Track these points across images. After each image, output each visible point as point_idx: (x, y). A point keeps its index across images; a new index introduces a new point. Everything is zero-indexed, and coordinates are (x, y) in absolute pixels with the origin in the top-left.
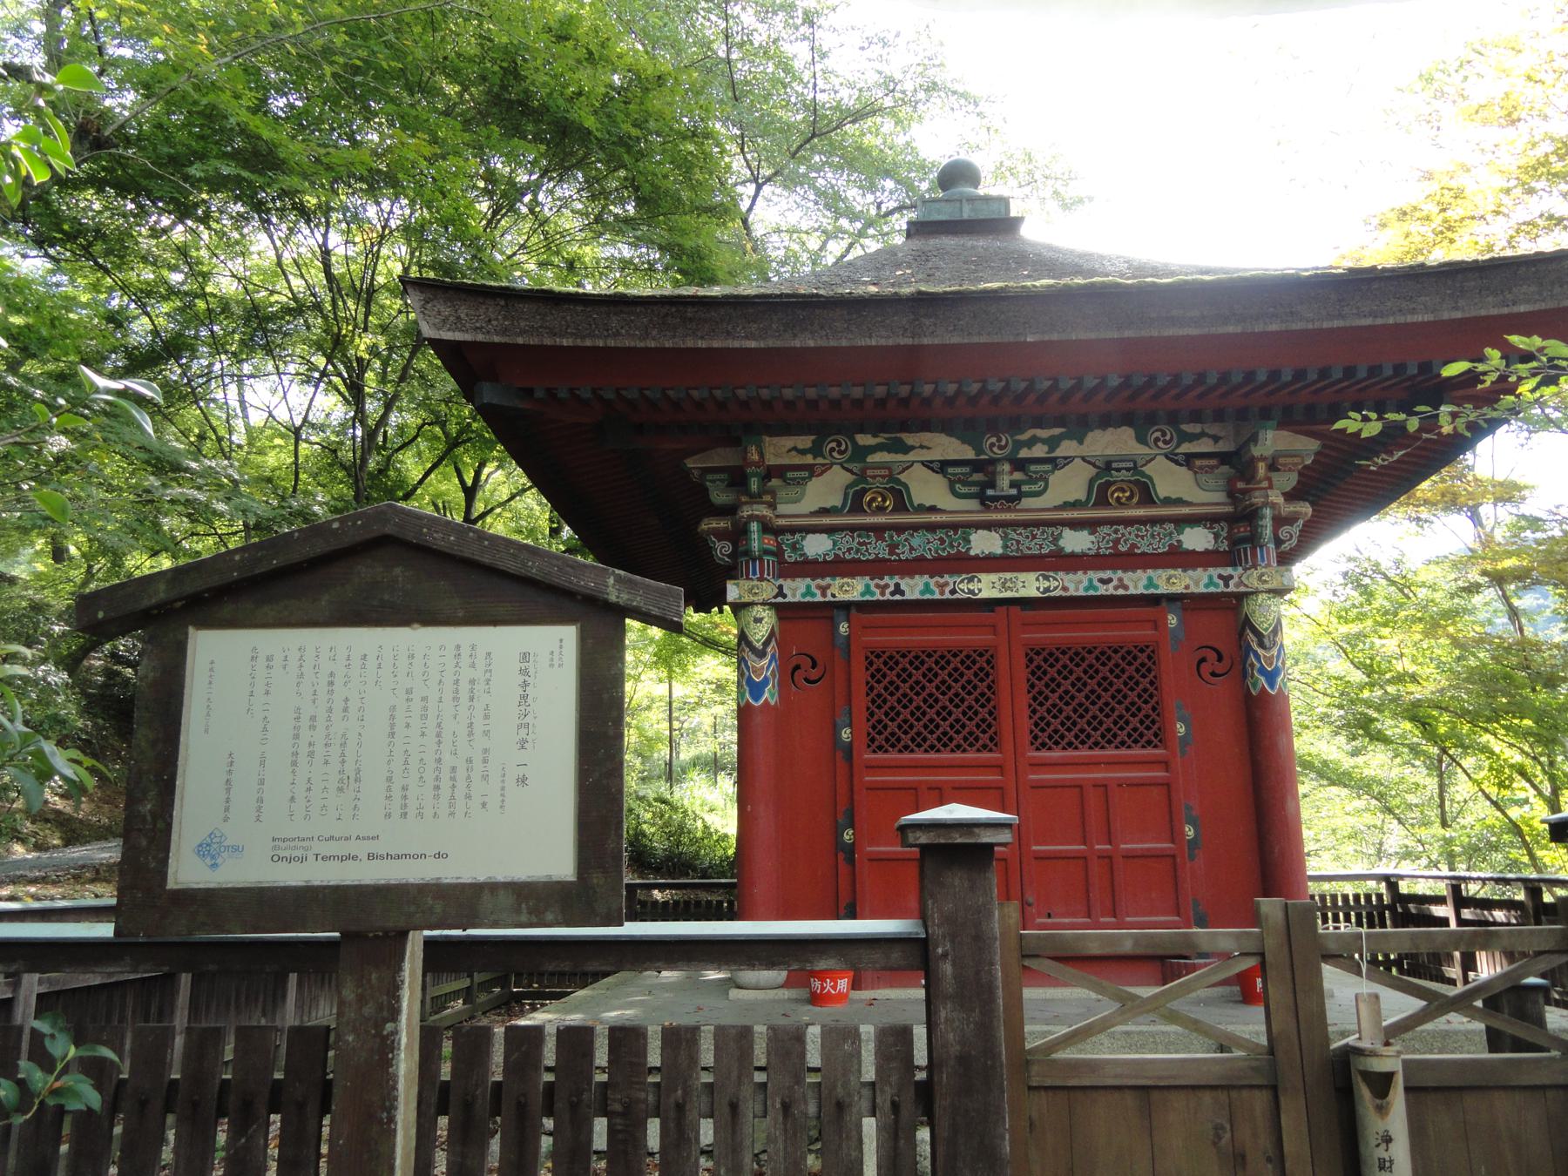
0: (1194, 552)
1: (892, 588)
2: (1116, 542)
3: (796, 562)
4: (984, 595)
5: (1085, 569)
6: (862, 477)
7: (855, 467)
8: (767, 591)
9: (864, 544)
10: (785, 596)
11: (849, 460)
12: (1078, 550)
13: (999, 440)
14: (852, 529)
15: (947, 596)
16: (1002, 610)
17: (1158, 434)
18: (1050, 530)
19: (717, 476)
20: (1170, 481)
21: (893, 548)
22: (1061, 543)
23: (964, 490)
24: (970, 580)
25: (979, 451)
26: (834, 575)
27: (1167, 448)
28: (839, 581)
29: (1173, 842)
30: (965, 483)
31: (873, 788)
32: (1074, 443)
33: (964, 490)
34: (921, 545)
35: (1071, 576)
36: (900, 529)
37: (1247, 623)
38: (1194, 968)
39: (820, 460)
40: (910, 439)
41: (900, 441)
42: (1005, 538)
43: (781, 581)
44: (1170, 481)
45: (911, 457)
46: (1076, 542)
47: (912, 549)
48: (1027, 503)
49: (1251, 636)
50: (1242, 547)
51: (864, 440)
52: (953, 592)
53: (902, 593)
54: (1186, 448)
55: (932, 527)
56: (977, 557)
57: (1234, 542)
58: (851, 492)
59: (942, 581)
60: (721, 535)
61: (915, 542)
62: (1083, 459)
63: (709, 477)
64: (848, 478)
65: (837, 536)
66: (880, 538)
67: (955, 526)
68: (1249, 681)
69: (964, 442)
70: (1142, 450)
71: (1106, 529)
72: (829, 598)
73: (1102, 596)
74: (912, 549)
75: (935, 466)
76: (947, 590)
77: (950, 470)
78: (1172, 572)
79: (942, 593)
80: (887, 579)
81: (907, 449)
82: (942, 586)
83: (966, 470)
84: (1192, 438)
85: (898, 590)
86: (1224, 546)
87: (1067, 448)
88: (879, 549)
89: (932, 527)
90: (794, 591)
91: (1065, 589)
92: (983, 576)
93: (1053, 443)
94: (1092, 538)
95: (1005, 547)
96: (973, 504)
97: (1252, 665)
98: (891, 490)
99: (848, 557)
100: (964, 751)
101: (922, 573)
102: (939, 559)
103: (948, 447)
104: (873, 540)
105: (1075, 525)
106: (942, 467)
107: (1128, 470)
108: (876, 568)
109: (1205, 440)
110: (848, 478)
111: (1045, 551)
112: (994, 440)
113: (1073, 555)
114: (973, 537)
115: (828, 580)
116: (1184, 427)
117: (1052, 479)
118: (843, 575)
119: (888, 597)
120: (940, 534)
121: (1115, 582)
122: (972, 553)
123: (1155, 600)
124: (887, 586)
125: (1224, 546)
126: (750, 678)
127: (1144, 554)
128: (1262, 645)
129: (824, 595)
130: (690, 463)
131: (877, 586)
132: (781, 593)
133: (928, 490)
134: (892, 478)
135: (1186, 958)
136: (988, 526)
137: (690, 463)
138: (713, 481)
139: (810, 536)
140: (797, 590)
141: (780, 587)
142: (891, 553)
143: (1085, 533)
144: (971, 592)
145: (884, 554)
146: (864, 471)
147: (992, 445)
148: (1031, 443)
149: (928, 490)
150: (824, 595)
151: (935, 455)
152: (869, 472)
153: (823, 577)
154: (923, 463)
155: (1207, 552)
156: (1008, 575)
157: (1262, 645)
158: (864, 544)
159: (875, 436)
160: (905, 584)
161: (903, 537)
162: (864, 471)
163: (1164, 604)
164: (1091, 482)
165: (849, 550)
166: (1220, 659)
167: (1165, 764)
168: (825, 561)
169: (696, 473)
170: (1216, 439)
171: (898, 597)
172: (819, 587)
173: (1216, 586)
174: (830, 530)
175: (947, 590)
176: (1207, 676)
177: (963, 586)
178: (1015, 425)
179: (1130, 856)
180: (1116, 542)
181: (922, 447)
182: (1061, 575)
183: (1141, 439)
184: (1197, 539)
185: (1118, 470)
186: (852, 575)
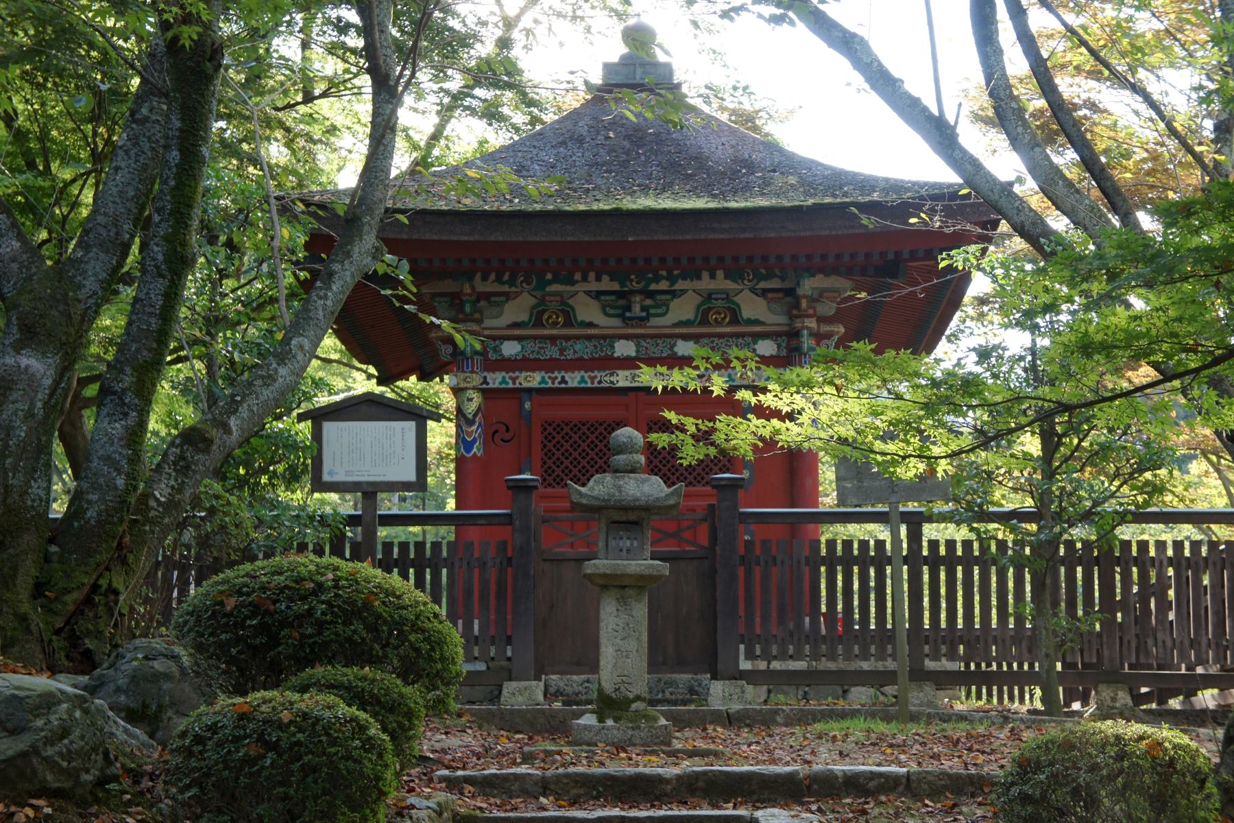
4: (620, 384)
7: (538, 294)
14: (535, 338)
15: (596, 385)
18: (668, 340)
21: (562, 351)
23: (612, 312)
24: (612, 375)
28: (524, 374)
33: (612, 312)
34: (582, 349)
36: (567, 338)
39: (513, 289)
42: (638, 345)
43: (485, 374)
47: (575, 352)
52: (600, 382)
53: (566, 383)
55: (589, 338)
61: (578, 347)
64: (533, 301)
65: (524, 343)
72: (517, 385)
74: (575, 352)
83: (613, 298)
85: (563, 381)
88: (552, 352)
92: (620, 372)
98: (562, 311)
102: (593, 359)
108: (549, 365)
111: (664, 355)
114: (616, 345)
115: (517, 373)
117: (672, 305)
118: (527, 370)
119: (556, 385)
129: (514, 383)
133: (588, 311)
134: (564, 303)
136: (627, 337)
139: (506, 343)
141: (485, 378)
142: (561, 354)
144: (612, 382)
145: (556, 355)
146: (543, 296)
149: (588, 311)
150: (514, 383)
154: (588, 293)
155: (772, 356)
160: (567, 377)
171: (563, 385)
172: (511, 378)
174: (519, 338)
177: (606, 378)
186: (533, 370)
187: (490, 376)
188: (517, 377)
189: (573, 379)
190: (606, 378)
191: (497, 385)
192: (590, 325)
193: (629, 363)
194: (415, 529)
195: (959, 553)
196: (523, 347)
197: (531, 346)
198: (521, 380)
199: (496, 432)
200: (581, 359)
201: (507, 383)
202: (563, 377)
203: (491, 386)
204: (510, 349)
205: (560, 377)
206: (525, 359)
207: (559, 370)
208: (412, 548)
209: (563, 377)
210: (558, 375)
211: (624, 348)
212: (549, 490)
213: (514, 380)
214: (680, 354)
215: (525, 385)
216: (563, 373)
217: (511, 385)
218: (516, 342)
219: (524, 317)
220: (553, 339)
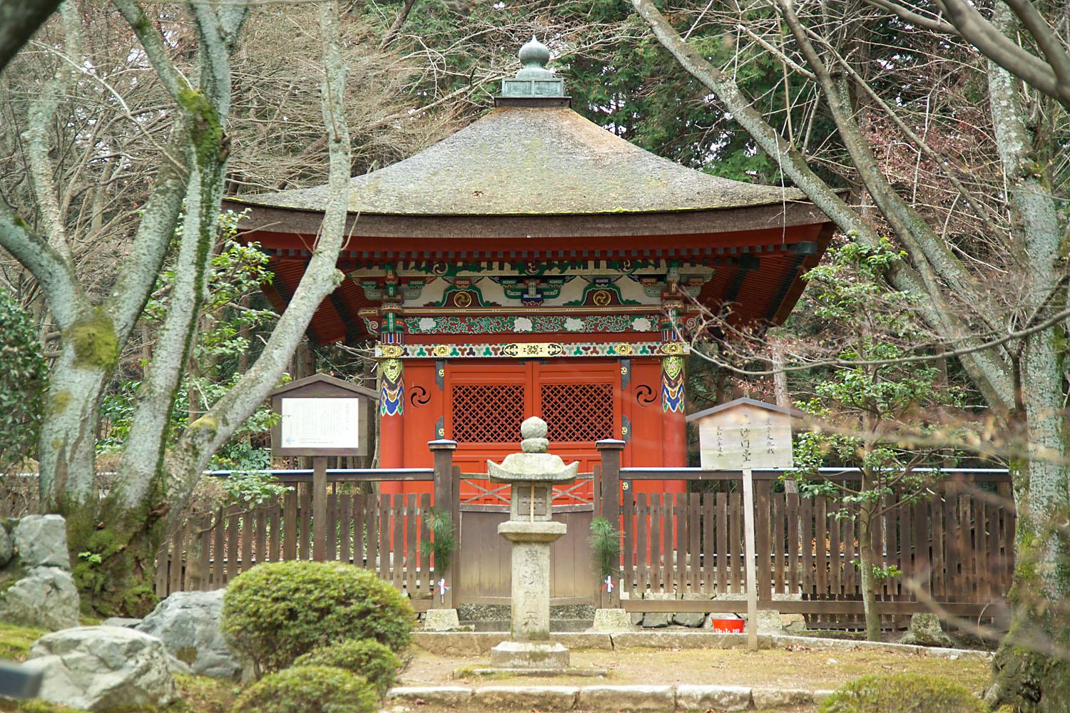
8: (398, 351)
12: (574, 330)
18: (559, 318)
19: (369, 283)
21: (470, 327)
23: (512, 294)
34: (486, 325)
39: (429, 275)
42: (534, 323)
46: (573, 325)
60: (372, 318)
63: (365, 283)
65: (438, 320)
72: (433, 356)
79: (496, 354)
85: (471, 352)
91: (564, 353)
94: (583, 323)
96: (517, 302)
105: (574, 316)
120: (497, 319)
129: (430, 354)
141: (406, 349)
150: (430, 354)
153: (586, 342)
160: (598, 347)
161: (478, 320)
171: (471, 356)
172: (493, 349)
173: (647, 352)
186: (446, 343)
190: (508, 350)
192: (494, 305)
196: (437, 323)
200: (486, 334)
203: (477, 356)
204: (427, 325)
206: (439, 334)
213: (430, 351)
214: (569, 330)
215: (440, 355)
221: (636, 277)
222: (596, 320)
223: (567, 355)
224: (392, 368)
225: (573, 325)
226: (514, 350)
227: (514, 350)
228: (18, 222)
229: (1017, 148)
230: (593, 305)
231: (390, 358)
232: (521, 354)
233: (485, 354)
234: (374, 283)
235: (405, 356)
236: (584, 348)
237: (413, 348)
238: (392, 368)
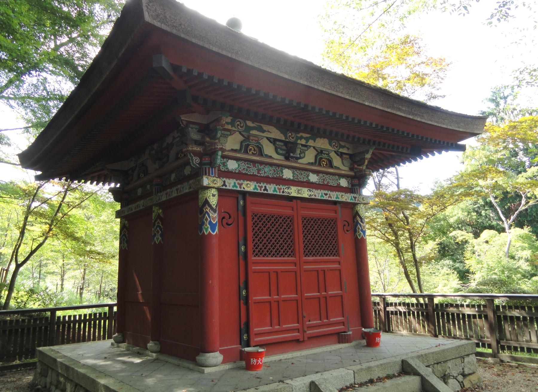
0: (343, 187)
1: (264, 188)
2: (324, 180)
3: (225, 171)
4: (292, 195)
5: (321, 189)
6: (247, 138)
7: (245, 134)
8: (219, 183)
9: (248, 167)
10: (226, 186)
11: (243, 131)
12: (314, 181)
13: (292, 135)
14: (245, 160)
15: (281, 194)
16: (294, 201)
17: (238, 123)
18: (306, 172)
19: (194, 126)
20: (337, 161)
21: (259, 170)
22: (309, 178)
23: (281, 152)
24: (288, 188)
25: (286, 138)
26: (244, 179)
27: (336, 149)
28: (246, 182)
29: (270, 296)
30: (282, 149)
31: (255, 272)
32: (312, 141)
33: (281, 152)
34: (267, 171)
35: (317, 191)
36: (261, 163)
37: (357, 214)
38: (419, 323)
39: (234, 129)
40: (265, 127)
41: (261, 127)
42: (293, 173)
43: (224, 179)
44: (337, 161)
45: (265, 134)
46: (313, 178)
47: (265, 172)
48: (300, 161)
49: (359, 219)
50: (204, 167)
51: (250, 124)
52: (283, 192)
53: (267, 191)
54: (341, 150)
55: (271, 165)
56: (285, 179)
57: (353, 185)
58: (244, 144)
59: (279, 187)
60: (196, 154)
61: (266, 169)
62: (314, 148)
63: (191, 126)
64: (241, 138)
65: (240, 163)
66: (254, 166)
67: (278, 166)
68: (357, 234)
69: (281, 133)
70: (330, 148)
71: (321, 175)
72: (242, 189)
73: (325, 200)
74: (265, 172)
75: (272, 140)
76: (281, 191)
77: (278, 143)
78: (248, 182)
79: (261, 190)
80: (262, 184)
81: (264, 131)
82: (280, 189)
83: (282, 144)
84: (343, 147)
85: (266, 189)
86: (350, 187)
87: (311, 143)
88: (253, 171)
89: (271, 165)
90: (230, 184)
91: (315, 196)
92: (292, 187)
93: (307, 140)
94: (317, 177)
95: (293, 176)
96: (282, 158)
97: (359, 228)
98: (257, 146)
99: (244, 172)
100: (284, 256)
101: (273, 183)
102: (273, 178)
103: (276, 134)
104: (252, 166)
105: (314, 172)
106: (274, 141)
107: (327, 154)
108: (257, 179)
109: (345, 148)
110: (241, 138)
111: (305, 180)
112: (290, 134)
113: (312, 183)
114: (284, 171)
115: (242, 181)
116: (341, 143)
117: (307, 153)
118: (247, 180)
119: (262, 191)
120: (274, 168)
121: (328, 195)
122: (284, 177)
123: (335, 203)
124: (262, 187)
125: (350, 187)
126: (210, 221)
127: (331, 186)
128: (362, 222)
129: (240, 187)
130: (183, 117)
131: (259, 186)
132: (224, 185)
133: (269, 149)
134: (258, 142)
135: (345, 332)
136: (289, 167)
137: (183, 117)
138: (192, 128)
139: (230, 161)
140: (231, 184)
141: (224, 182)
142: (258, 173)
143: (315, 175)
144: (289, 193)
145: (256, 173)
146: (249, 136)
147: (290, 136)
148: (301, 138)
149: (269, 149)
150: (240, 187)
151: (272, 136)
152: (251, 138)
153: (240, 180)
154: (267, 138)
155: (346, 188)
156: (299, 188)
157: (362, 222)
158: (248, 167)
159: (253, 123)
160: (268, 186)
161: (262, 167)
162: (249, 136)
163: (338, 204)
164: (316, 157)
165: (244, 169)
166: (230, 217)
167: (339, 263)
168: (235, 173)
169: (184, 123)
170: (348, 149)
171: (266, 192)
172: (238, 184)
173: (257, 190)
174: (237, 159)
175: (281, 191)
176: (346, 231)
177: (286, 190)
178: (298, 131)
179: (285, 300)
180: (324, 180)
181: (269, 132)
182: (314, 190)
183: (330, 144)
184: (344, 183)
185: (324, 154)
186: (250, 181)
187: (227, 181)
188: (242, 184)
189: (270, 188)
190: (286, 190)
191: (231, 188)
192: (271, 157)
193: (290, 183)
194: (94, 309)
195: (83, 318)
196: (239, 165)
197: (244, 165)
198: (244, 186)
199: (224, 218)
200: (267, 177)
201: (237, 187)
202: (265, 187)
203: (228, 188)
204: (232, 165)
205: (264, 186)
206: (240, 173)
207: (264, 182)
208: (88, 315)
209: (265, 187)
210: (263, 185)
211: (288, 174)
212: (257, 258)
213: (241, 185)
214: (311, 181)
215: (247, 189)
216: (265, 184)
217: (239, 189)
218: (235, 162)
219: (237, 147)
220: (254, 162)
221: (272, 140)
222: (324, 176)
223: (317, 197)
224: (214, 195)
225: (313, 178)
226: (289, 191)
227: (289, 191)
228: (525, 171)
229: (95, 11)
230: (246, 152)
231: (213, 188)
232: (294, 194)
233: (233, 187)
234: (197, 127)
235: (224, 187)
236: (325, 194)
237: (270, 186)
238: (214, 195)
